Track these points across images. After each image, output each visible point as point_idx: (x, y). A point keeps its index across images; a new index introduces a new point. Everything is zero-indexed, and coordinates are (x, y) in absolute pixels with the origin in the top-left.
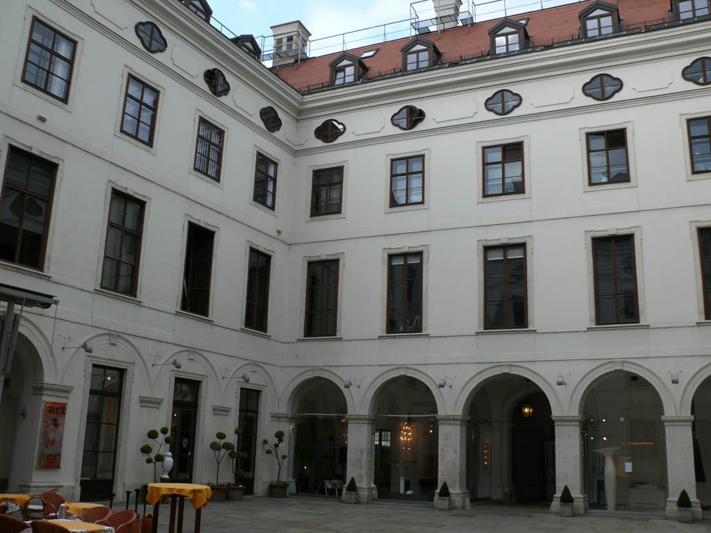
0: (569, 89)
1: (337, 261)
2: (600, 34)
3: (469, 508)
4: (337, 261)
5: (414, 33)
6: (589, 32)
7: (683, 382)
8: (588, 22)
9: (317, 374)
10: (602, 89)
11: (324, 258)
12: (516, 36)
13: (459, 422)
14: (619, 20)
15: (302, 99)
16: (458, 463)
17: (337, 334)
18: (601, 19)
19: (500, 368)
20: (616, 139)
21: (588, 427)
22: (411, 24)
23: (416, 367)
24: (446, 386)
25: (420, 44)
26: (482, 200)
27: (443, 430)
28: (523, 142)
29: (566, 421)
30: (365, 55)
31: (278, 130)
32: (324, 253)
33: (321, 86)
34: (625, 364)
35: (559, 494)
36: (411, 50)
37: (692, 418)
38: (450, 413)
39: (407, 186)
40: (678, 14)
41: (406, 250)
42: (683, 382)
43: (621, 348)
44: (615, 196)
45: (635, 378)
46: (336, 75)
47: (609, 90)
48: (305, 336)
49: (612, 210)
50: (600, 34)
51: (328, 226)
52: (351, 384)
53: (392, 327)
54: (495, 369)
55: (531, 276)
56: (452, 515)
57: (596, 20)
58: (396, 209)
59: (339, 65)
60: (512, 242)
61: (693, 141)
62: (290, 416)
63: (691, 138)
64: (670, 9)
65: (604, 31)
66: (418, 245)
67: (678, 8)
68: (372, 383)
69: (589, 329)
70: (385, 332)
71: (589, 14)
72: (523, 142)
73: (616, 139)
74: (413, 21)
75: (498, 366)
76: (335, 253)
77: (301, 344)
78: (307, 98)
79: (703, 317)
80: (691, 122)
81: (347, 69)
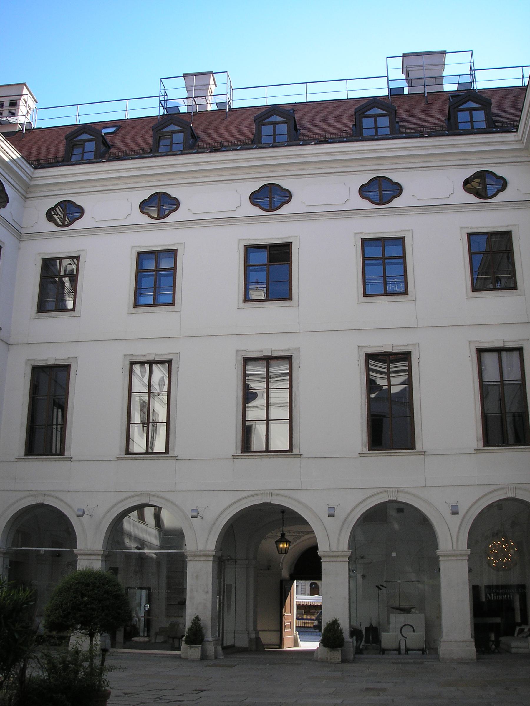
0: (235, 197)
1: (67, 368)
2: (82, 159)
3: (221, 657)
4: (67, 368)
5: (162, 112)
6: (263, 138)
7: (341, 514)
8: (364, 120)
9: (40, 500)
10: (381, 191)
11: (51, 362)
12: (286, 126)
13: (100, 558)
14: (296, 129)
15: (33, 173)
16: (209, 605)
17: (66, 453)
18: (473, 112)
19: (260, 497)
20: (279, 255)
21: (222, 560)
22: (160, 101)
23: (162, 494)
24: (198, 517)
25: (175, 125)
26: (242, 304)
27: (192, 568)
28: (291, 243)
29: (334, 556)
30: (104, 131)
31: (4, 207)
32: (51, 356)
33: (54, 161)
34: (46, 497)
35: (61, 634)
36: (462, 107)
37: (349, 553)
38: (201, 547)
39: (155, 285)
40: (361, 129)
41: (269, 354)
42: (341, 514)
43: (391, 476)
44: (274, 314)
45: (284, 511)
46: (73, 150)
47: (491, 189)
48: (25, 455)
49: (387, 323)
50: (472, 128)
51: (55, 324)
52: (84, 513)
53: (31, 449)
54: (255, 497)
55: (297, 394)
56: (209, 666)
57: (272, 127)
58: (141, 310)
59: (265, 121)
60: (275, 354)
61: (366, 262)
62: (5, 550)
63: (364, 259)
64: (447, 117)
65: (381, 132)
66: (166, 353)
67: (456, 117)
68: (108, 512)
69: (119, 458)
70: (240, 451)
71: (365, 112)
72: (291, 243)
73: (279, 255)
74: (162, 98)
75: (257, 495)
76: (66, 357)
77: (238, 461)
78: (40, 172)
79: (481, 444)
80: (366, 242)
81: (87, 144)
